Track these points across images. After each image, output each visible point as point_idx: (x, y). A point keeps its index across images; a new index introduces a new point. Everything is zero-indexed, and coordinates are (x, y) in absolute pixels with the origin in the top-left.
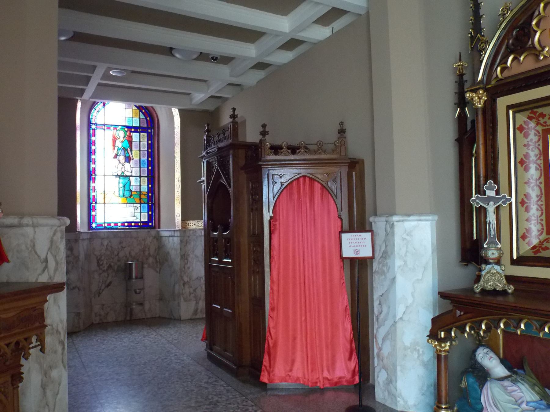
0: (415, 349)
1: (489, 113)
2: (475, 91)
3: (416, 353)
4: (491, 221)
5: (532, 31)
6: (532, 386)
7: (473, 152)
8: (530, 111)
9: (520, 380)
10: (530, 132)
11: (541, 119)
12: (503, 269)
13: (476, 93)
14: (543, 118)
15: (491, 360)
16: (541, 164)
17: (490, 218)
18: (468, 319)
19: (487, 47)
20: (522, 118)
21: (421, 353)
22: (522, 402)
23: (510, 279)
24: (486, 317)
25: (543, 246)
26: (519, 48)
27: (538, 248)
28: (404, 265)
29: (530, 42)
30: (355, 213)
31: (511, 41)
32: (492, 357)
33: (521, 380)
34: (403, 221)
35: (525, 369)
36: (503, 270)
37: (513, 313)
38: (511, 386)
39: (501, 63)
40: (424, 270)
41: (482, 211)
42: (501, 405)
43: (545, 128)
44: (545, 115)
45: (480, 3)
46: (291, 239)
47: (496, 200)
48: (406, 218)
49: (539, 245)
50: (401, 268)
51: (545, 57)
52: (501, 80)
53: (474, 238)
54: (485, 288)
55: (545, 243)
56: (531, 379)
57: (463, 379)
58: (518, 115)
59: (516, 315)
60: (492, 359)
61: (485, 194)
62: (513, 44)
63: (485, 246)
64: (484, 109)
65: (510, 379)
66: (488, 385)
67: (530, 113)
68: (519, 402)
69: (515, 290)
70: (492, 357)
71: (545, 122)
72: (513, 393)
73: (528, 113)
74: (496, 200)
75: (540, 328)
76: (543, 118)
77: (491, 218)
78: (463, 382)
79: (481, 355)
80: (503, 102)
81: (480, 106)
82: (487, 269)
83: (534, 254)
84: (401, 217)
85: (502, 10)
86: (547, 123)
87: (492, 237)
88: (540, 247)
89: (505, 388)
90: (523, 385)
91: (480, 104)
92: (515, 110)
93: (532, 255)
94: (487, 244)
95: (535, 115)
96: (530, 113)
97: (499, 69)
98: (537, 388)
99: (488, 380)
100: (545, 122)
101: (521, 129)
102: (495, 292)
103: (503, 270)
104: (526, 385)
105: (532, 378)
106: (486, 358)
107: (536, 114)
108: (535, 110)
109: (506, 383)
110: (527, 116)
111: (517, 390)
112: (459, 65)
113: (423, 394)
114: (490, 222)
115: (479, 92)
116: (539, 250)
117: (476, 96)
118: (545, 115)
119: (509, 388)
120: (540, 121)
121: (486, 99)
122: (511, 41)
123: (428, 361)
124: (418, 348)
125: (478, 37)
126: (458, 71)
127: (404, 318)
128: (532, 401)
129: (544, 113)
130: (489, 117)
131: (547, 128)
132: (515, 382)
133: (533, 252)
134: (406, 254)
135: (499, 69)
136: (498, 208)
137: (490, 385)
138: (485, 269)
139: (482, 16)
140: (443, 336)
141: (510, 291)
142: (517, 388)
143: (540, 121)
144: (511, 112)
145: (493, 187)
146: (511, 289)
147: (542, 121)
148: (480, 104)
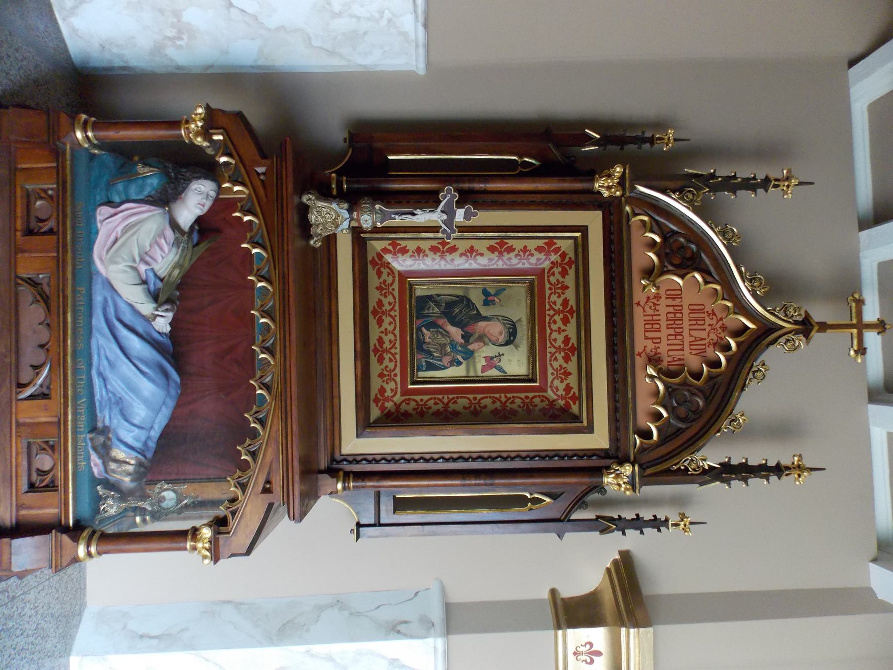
0: (180, 31)
1: (583, 198)
2: (621, 183)
3: (174, 34)
4: (416, 217)
5: (685, 271)
6: (177, 265)
7: (527, 157)
8: (573, 259)
9: (181, 248)
10: (543, 254)
11: (560, 269)
12: (344, 231)
13: (618, 183)
14: (560, 273)
15: (199, 206)
16: (497, 265)
17: (421, 214)
18: (255, 191)
19: (685, 203)
20: (566, 246)
21: (178, 43)
22: (147, 263)
23: (330, 241)
24: (262, 222)
25: (382, 269)
26: (668, 251)
27: (380, 262)
28: (333, 12)
29: (670, 268)
30: (409, 369)
31: (682, 240)
32: (204, 207)
33: (182, 250)
34: (415, 12)
35: (202, 245)
36: (342, 231)
37: (279, 270)
38: (168, 241)
39: (654, 224)
40: (329, 51)
41: (430, 200)
42: (129, 238)
43: (546, 271)
44: (563, 277)
45: (756, 192)
46: (294, 370)
47: (449, 222)
48: (421, 18)
49: (384, 262)
50: (327, 6)
51: (645, 287)
52: (628, 220)
53: (390, 156)
54: (310, 210)
55: (387, 270)
56: (188, 258)
57: (151, 169)
58: (571, 242)
59: (276, 277)
60: (202, 207)
61: (458, 207)
62: (676, 241)
63: (377, 206)
64: (591, 192)
65: (178, 235)
66: (157, 211)
67: (570, 258)
68: (148, 259)
69: (314, 249)
70: (204, 207)
71: (553, 274)
72: (157, 247)
73: (571, 254)
74: (449, 222)
75: (263, 311)
76: (560, 273)
77: (423, 217)
78: (146, 169)
79: (203, 188)
80: (593, 220)
81: (597, 185)
82: (341, 211)
83: (370, 261)
84: (423, 8)
85: (733, 231)
86: (552, 276)
87: (393, 216)
88: (381, 265)
89: (162, 234)
90: (176, 254)
91: (599, 186)
92: (580, 240)
93: (369, 258)
94: (380, 209)
95: (566, 264)
96: (570, 258)
97: (646, 218)
98: (177, 272)
99: (165, 208)
100: (553, 274)
101: (551, 241)
102: (305, 227)
103: (342, 231)
104: (177, 257)
105: (190, 260)
106: (200, 197)
107: (572, 400)
108: (573, 266)
109: (170, 234)
110: (566, 252)
111: (164, 252)
112: (669, 139)
113: (103, 47)
114: (414, 214)
115: (618, 191)
116: (377, 264)
117: (613, 183)
118: (563, 277)
119: (163, 241)
120: (557, 267)
121: (605, 195)
122: (682, 240)
123: (166, 55)
124: (185, 37)
125: (705, 189)
126: (661, 136)
127: (232, 10)
128: (156, 272)
129: (567, 277)
130: (576, 198)
131: (546, 275)
132: (176, 243)
133: (373, 258)
134: (355, 16)
135: (646, 218)
136: (435, 229)
137: (158, 214)
138: (342, 208)
139: (735, 193)
140: (216, 138)
141: (312, 242)
142: (167, 252)
143: (557, 267)
144: (578, 234)
145: (469, 217)
146: (316, 243)
147: (557, 270)
148: (599, 186)
